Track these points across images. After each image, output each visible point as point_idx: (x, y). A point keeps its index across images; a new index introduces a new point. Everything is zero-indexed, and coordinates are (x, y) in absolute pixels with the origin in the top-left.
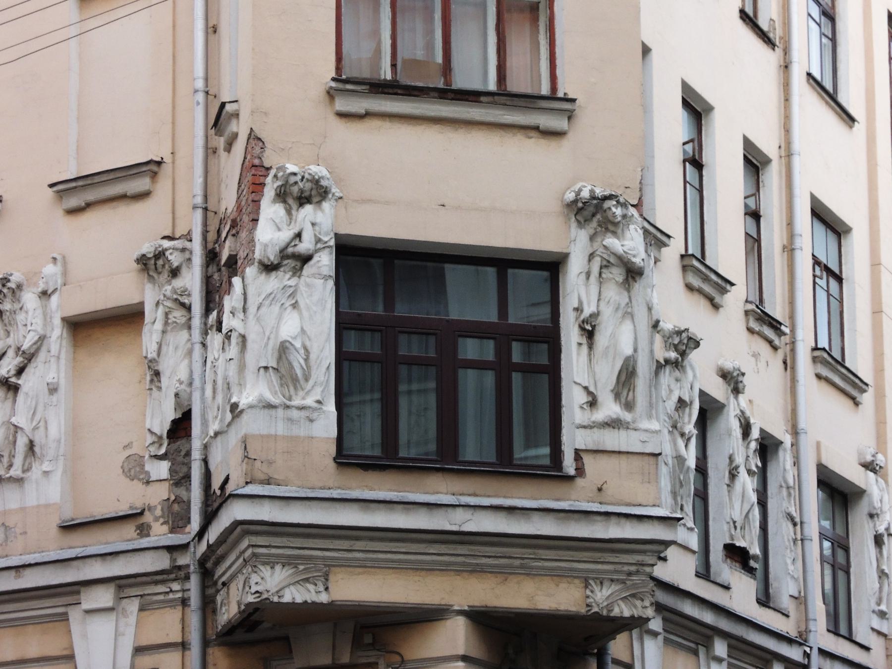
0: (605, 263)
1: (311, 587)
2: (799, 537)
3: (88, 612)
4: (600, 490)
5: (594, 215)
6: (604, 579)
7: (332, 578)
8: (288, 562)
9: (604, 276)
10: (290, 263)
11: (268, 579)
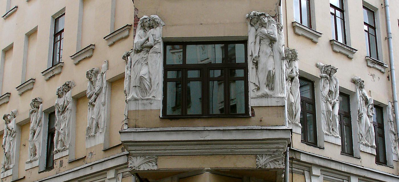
0: (261, 38)
1: (150, 164)
2: (397, 139)
3: (109, 179)
4: (261, 121)
5: (257, 22)
6: (263, 154)
7: (159, 160)
8: (143, 155)
9: (261, 43)
10: (146, 49)
11: (135, 162)
